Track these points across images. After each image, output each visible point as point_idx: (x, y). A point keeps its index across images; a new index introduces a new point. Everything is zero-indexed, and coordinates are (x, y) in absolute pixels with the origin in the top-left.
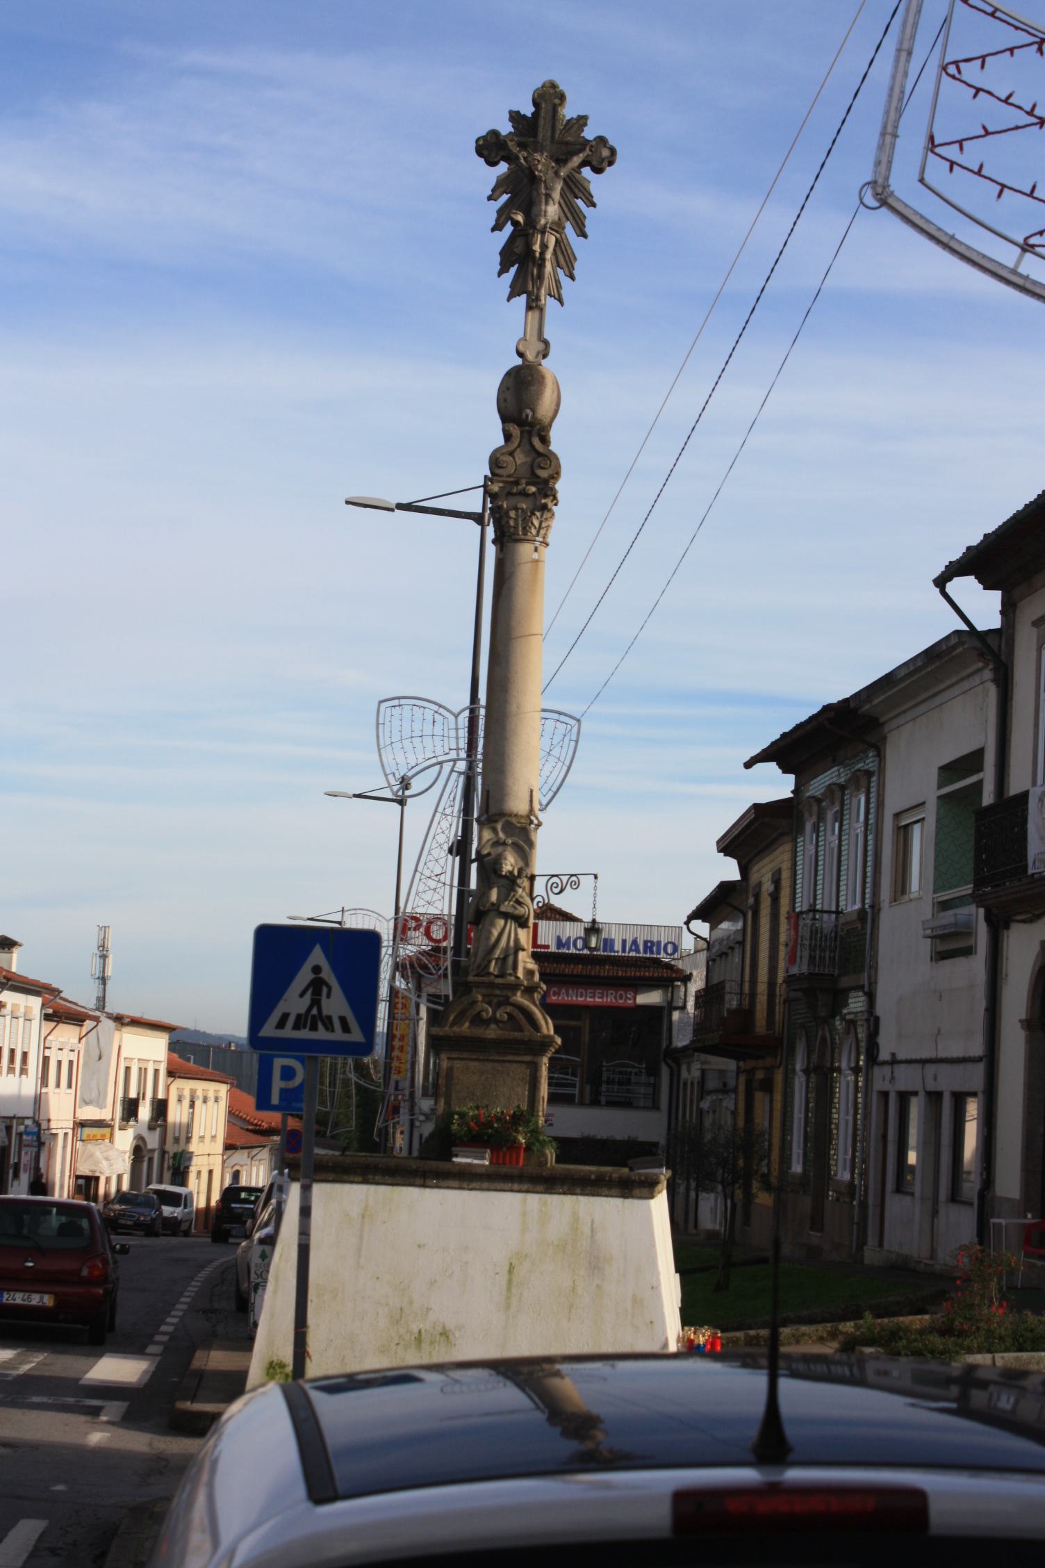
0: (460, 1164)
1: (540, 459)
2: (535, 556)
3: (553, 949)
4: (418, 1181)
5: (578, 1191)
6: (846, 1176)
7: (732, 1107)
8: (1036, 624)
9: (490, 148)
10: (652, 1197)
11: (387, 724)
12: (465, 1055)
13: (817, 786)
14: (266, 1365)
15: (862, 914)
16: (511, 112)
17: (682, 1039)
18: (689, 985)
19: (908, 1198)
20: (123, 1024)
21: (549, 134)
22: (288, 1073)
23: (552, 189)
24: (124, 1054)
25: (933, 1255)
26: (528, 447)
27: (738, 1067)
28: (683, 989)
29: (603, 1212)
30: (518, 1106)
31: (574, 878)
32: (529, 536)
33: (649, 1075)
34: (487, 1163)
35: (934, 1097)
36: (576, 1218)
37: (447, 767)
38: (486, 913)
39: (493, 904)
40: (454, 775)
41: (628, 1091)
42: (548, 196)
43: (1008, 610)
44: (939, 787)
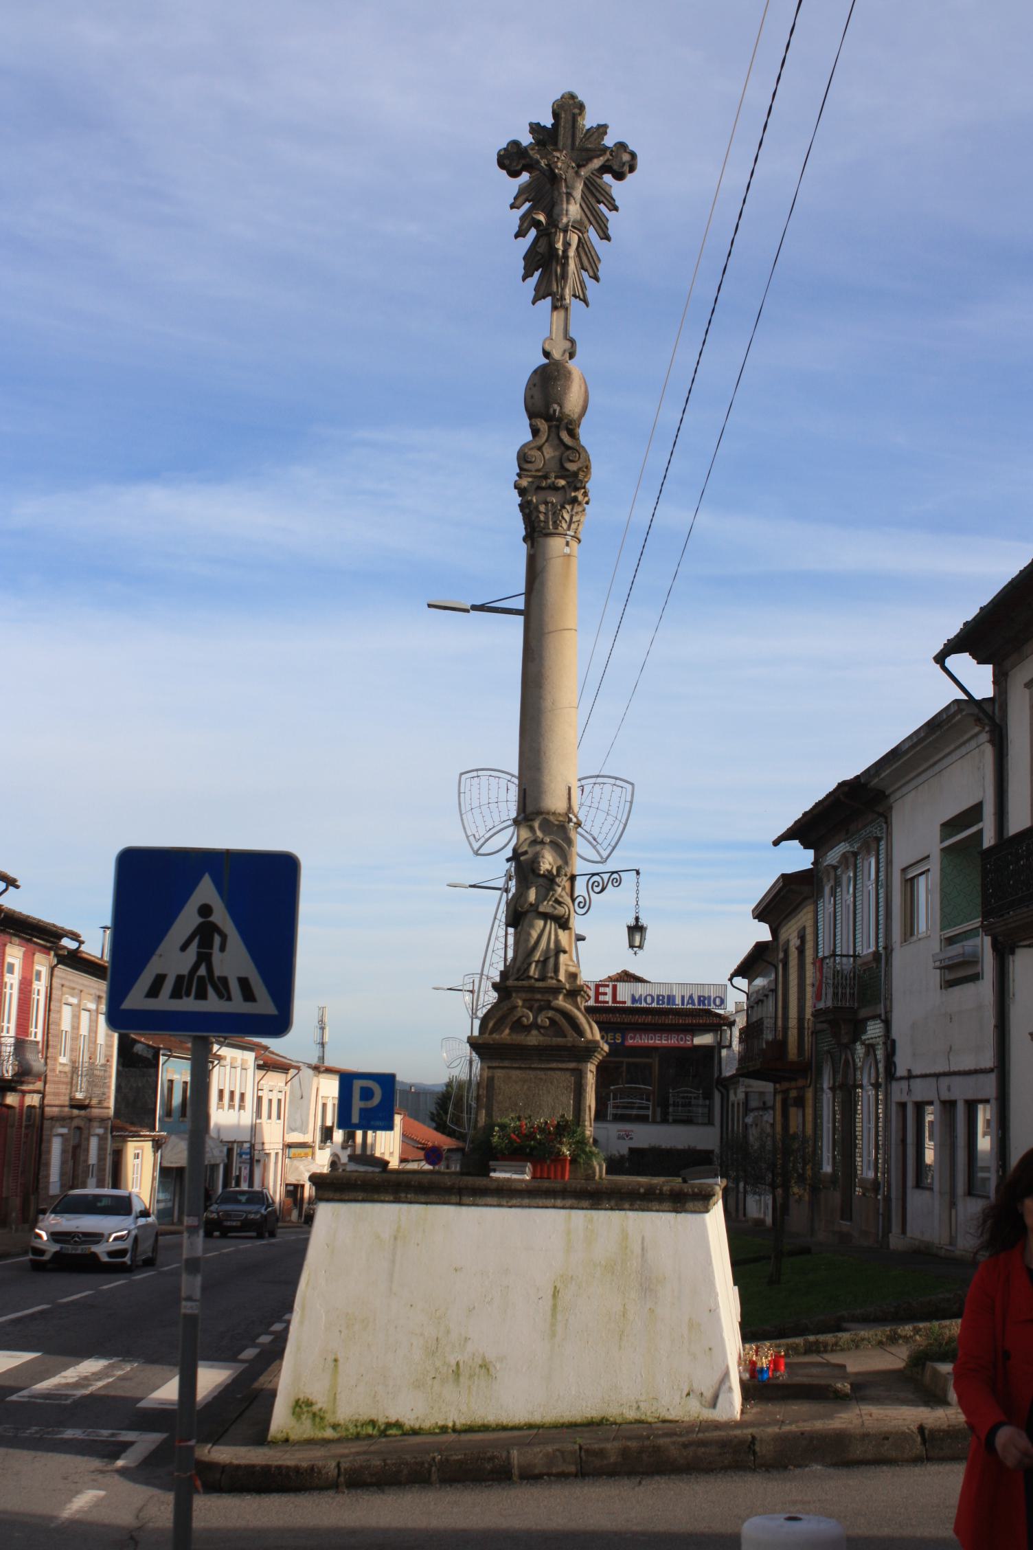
0: (497, 1179)
1: (569, 452)
2: (567, 550)
3: (629, 1004)
4: (454, 1199)
5: (627, 1206)
6: (871, 1175)
8: (1027, 685)
9: (512, 159)
10: (707, 1211)
11: (468, 793)
12: (506, 1064)
13: (833, 857)
14: (291, 1403)
15: (876, 955)
16: (531, 124)
17: (729, 1070)
19: (927, 1193)
20: (319, 1072)
21: (569, 141)
22: (367, 1094)
23: (573, 188)
24: (320, 1094)
25: (952, 1241)
26: (556, 442)
29: (654, 1227)
30: (563, 1116)
31: (615, 876)
32: (560, 530)
33: (705, 1099)
35: (949, 1106)
36: (625, 1236)
38: (525, 914)
39: (531, 905)
41: (689, 1111)
42: (569, 195)
43: (1000, 680)
44: (942, 841)
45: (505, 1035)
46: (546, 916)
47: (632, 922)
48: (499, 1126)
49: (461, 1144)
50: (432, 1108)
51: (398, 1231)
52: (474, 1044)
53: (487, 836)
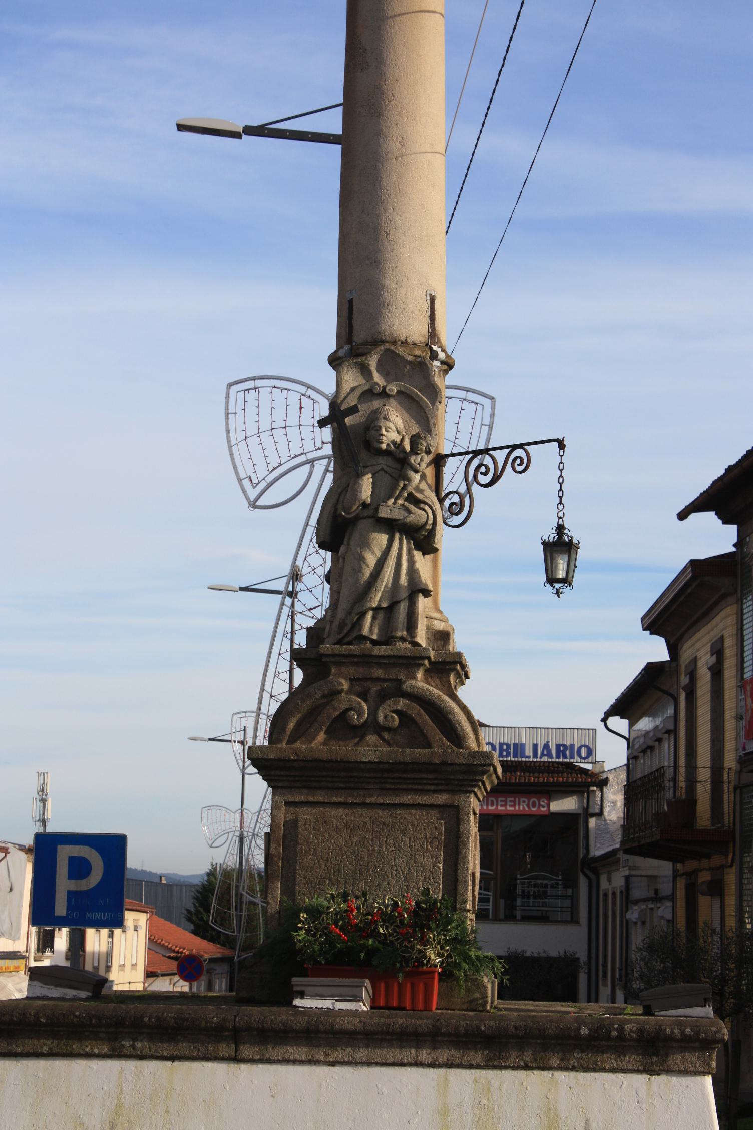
0: (308, 1011)
4: (225, 1049)
5: (555, 1062)
7: (669, 916)
11: (240, 413)
12: (319, 797)
18: (605, 790)
22: (79, 868)
27: (675, 871)
28: (599, 794)
30: (426, 892)
31: (519, 452)
33: (566, 887)
39: (364, 505)
41: (544, 905)
45: (318, 743)
46: (391, 527)
47: (551, 535)
48: (306, 910)
50: (189, 904)
51: (117, 1114)
53: (270, 479)
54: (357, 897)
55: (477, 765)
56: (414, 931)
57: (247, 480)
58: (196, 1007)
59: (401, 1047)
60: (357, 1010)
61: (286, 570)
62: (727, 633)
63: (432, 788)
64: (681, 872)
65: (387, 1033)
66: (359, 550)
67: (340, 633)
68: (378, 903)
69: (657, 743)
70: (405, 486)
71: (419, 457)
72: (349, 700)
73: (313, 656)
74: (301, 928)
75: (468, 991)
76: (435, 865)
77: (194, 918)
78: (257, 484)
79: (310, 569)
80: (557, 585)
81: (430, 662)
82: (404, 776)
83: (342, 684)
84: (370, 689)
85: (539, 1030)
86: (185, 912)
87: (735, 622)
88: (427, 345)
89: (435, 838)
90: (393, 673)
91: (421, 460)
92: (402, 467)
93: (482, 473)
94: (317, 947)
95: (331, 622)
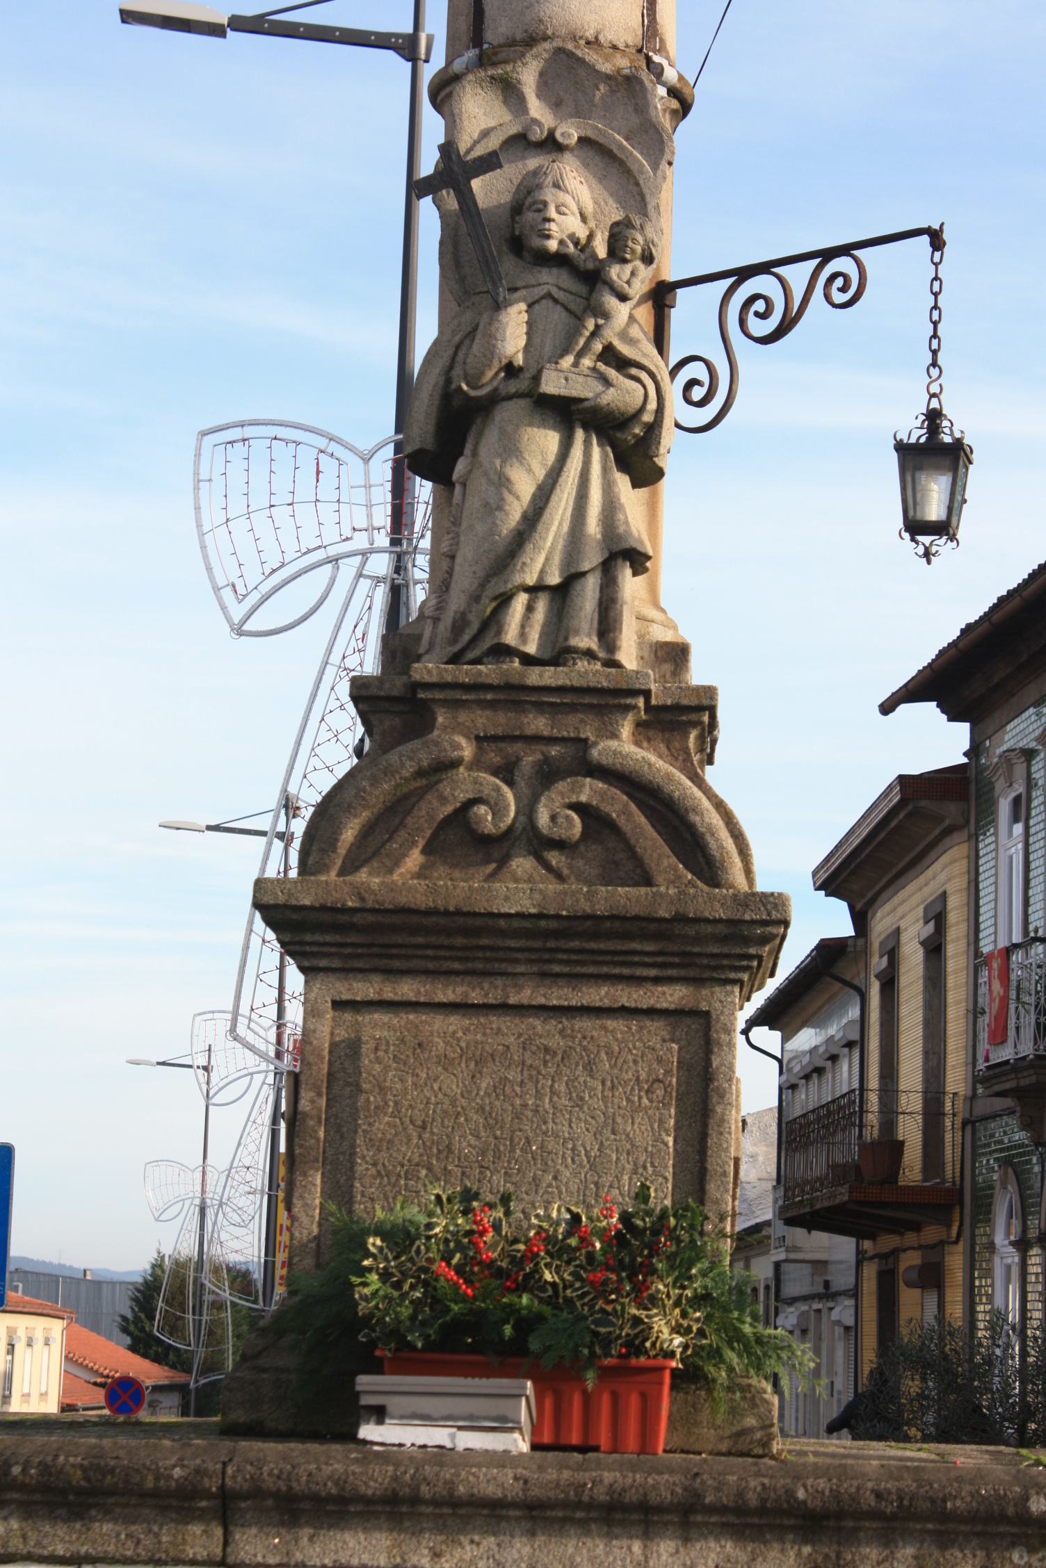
0: (391, 1454)
7: (850, 1322)
12: (407, 989)
27: (859, 1252)
30: (642, 1195)
31: (842, 264)
34: (520, 1444)
37: (348, 568)
38: (485, 406)
39: (511, 370)
40: (365, 584)
45: (407, 876)
46: (566, 413)
47: (915, 433)
49: (180, 1378)
50: (125, 1308)
52: (279, 911)
53: (266, 587)
54: (491, 1206)
55: (753, 922)
56: (620, 1280)
57: (229, 588)
58: (133, 1442)
59: (610, 1536)
60: (506, 1452)
61: (272, 799)
62: (950, 888)
63: (653, 972)
64: (870, 1253)
65: (579, 1505)
66: (498, 462)
67: (454, 641)
68: (537, 1216)
69: (829, 1063)
70: (597, 327)
71: (628, 268)
72: (476, 782)
73: (395, 693)
74: (369, 1270)
75: (734, 1411)
76: (658, 1139)
77: (132, 1328)
78: (245, 596)
79: (330, 735)
80: (926, 540)
81: (649, 708)
82: (593, 945)
83: (458, 747)
84: (519, 759)
85: (933, 1501)
86: (119, 1319)
87: (965, 870)
88: (640, 51)
89: (658, 1080)
90: (571, 725)
91: (633, 274)
92: (591, 291)
93: (757, 314)
94: (405, 1311)
95: (436, 620)
